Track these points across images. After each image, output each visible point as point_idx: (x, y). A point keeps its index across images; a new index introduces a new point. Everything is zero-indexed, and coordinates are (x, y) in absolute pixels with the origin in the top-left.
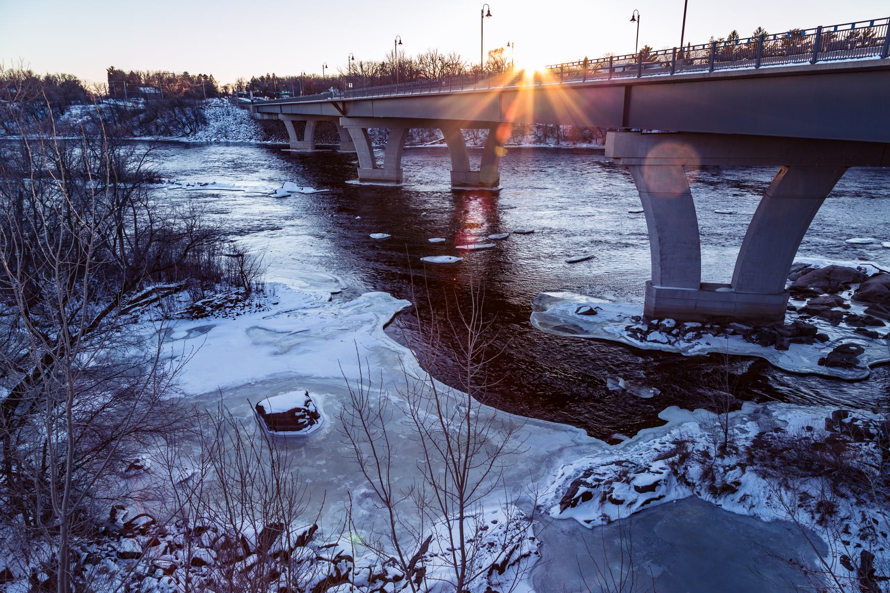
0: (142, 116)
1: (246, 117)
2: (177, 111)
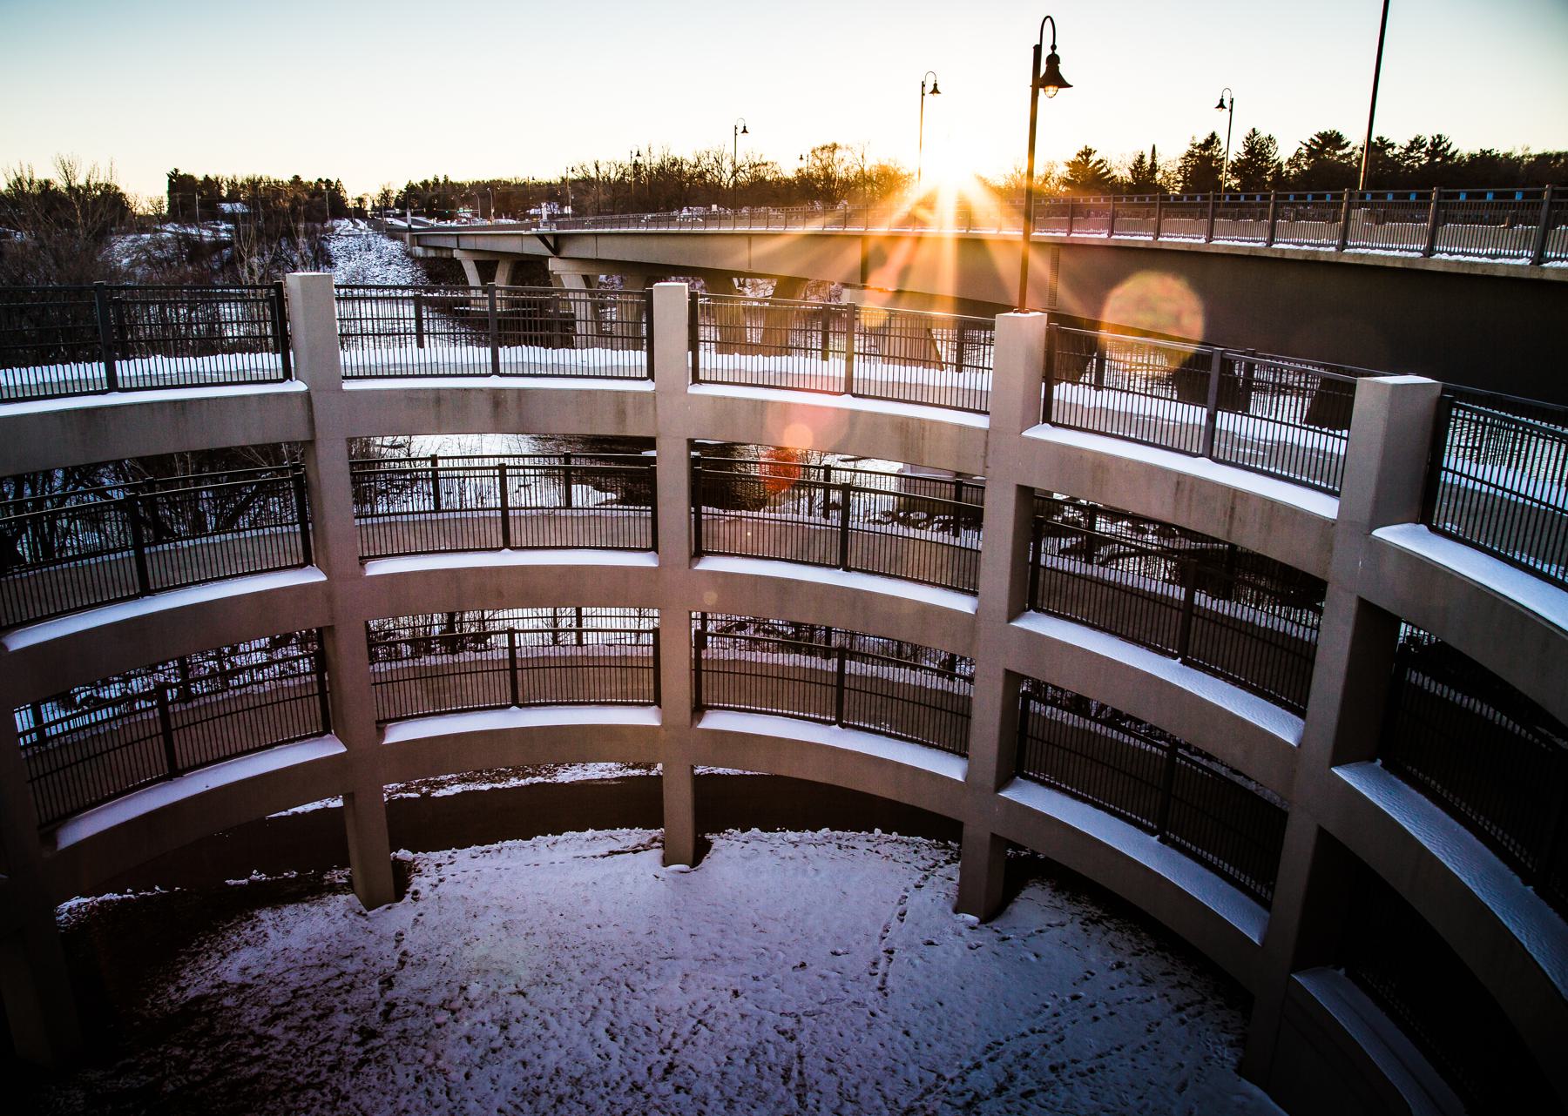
0: (226, 252)
1: (397, 253)
2: (284, 244)
